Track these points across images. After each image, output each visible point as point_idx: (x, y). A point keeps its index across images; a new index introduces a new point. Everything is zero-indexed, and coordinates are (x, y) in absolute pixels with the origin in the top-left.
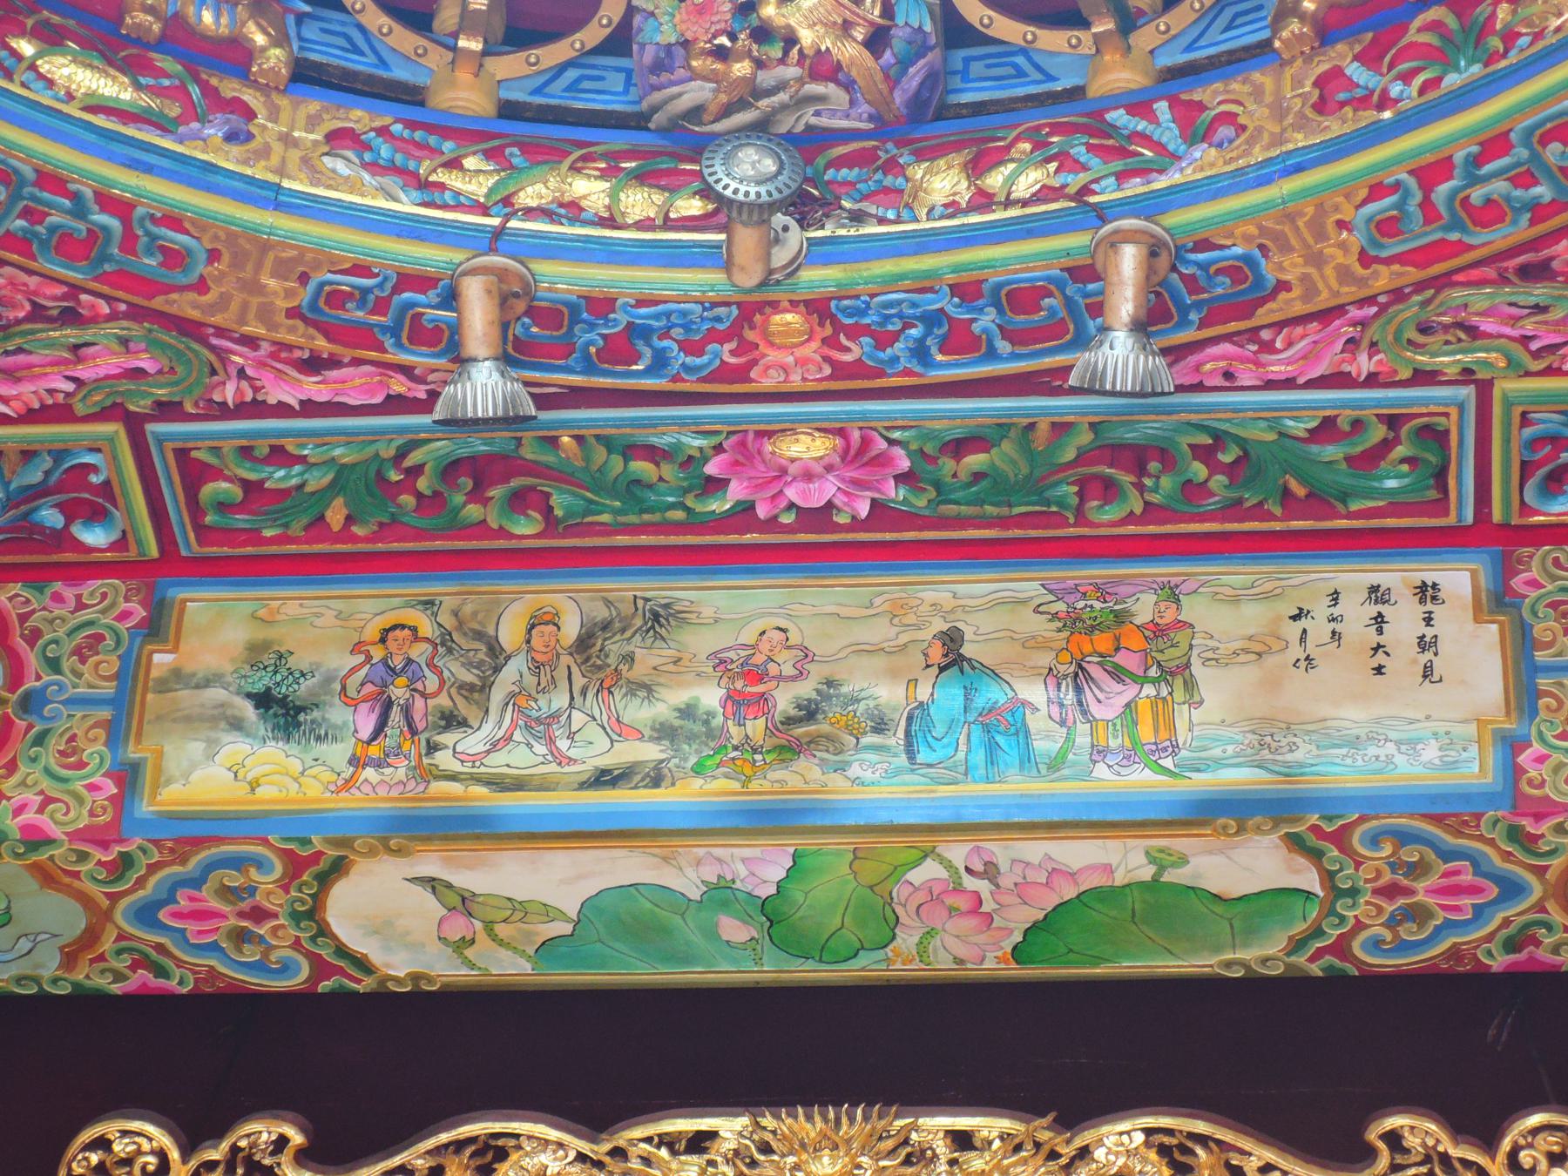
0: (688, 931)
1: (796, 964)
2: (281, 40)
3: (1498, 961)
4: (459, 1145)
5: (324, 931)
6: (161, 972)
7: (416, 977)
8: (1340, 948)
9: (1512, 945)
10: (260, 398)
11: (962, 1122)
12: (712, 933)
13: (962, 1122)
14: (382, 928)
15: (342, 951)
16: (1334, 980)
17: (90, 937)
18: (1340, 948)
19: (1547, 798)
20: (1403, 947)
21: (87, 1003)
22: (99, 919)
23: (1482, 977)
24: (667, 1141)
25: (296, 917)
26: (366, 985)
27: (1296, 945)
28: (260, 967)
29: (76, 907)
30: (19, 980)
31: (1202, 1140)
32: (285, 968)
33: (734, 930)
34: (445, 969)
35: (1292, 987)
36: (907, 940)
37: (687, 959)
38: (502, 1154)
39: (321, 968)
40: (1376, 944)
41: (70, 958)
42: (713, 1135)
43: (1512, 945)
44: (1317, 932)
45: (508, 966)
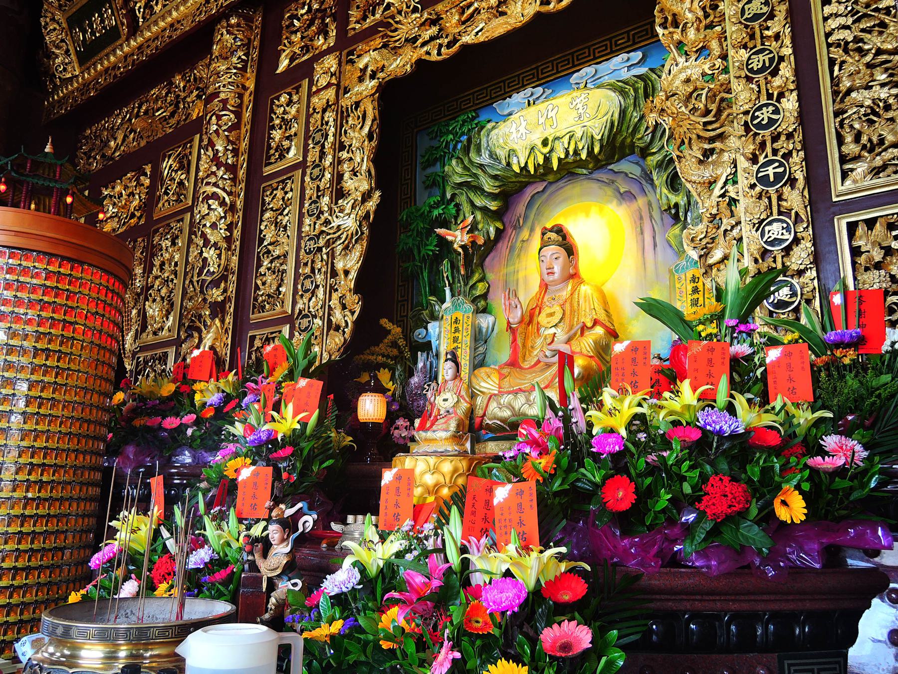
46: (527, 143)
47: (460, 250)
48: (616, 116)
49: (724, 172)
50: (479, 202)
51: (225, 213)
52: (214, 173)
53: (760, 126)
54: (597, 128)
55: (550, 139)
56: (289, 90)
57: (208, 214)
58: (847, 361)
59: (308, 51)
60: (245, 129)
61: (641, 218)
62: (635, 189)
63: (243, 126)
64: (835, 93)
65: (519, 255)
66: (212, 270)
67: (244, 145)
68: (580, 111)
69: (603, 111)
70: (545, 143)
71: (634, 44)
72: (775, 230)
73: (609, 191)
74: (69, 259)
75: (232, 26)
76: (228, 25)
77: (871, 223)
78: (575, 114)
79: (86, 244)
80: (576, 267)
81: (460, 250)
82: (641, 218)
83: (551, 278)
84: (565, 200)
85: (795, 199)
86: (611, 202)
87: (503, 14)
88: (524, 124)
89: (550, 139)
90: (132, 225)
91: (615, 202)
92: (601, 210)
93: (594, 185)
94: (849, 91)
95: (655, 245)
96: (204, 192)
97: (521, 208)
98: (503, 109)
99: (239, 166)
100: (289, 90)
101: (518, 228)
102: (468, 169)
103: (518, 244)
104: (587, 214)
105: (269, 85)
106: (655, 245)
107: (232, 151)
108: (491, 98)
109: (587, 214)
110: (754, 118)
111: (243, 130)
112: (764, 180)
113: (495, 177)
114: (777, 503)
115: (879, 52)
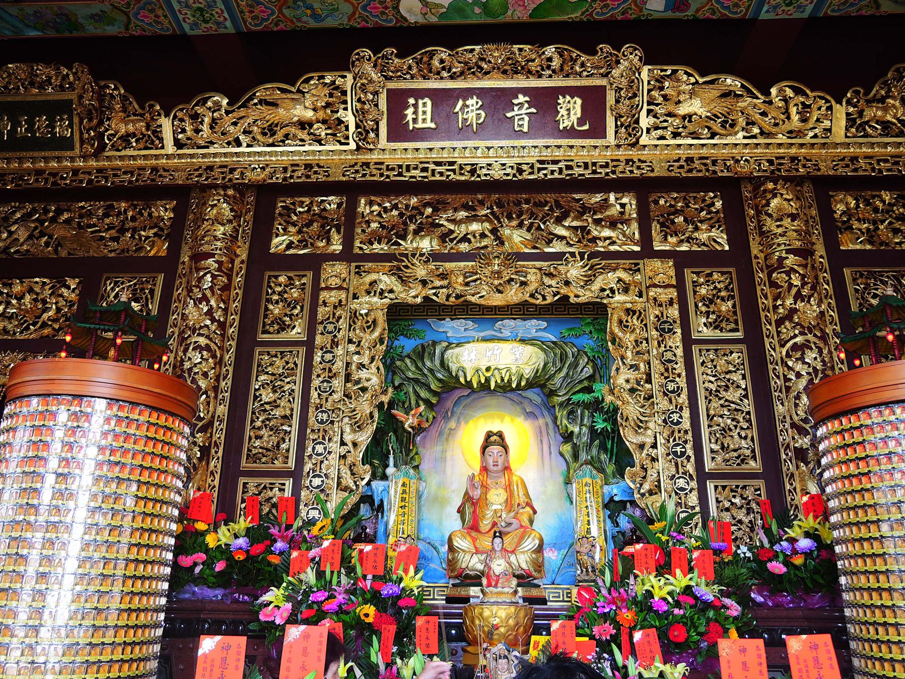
0: (468, 10)
1: (488, 19)
2: (892, 332)
3: (620, 18)
4: (426, 52)
5: (399, 12)
6: (367, 22)
7: (416, 22)
8: (591, 15)
9: (623, 14)
10: (244, 533)
11: (521, 46)
12: (473, 11)
13: (521, 46)
14: (410, 11)
15: (402, 16)
16: (589, 22)
17: (354, 14)
18: (591, 15)
19: (812, 91)
20: (603, 14)
21: (352, 29)
22: (356, 8)
23: (617, 21)
24: (466, 50)
25: (394, 8)
26: (406, 25)
27: (583, 13)
28: (386, 21)
29: (351, 6)
30: (340, 24)
31: (566, 49)
32: (391, 21)
33: (477, 10)
34: (421, 20)
35: (581, 22)
36: (510, 13)
37: (467, 17)
38: (434, 55)
39: (398, 21)
40: (598, 13)
41: (349, 20)
42: (474, 50)
43: (623, 14)
44: (587, 10)
45: (433, 19)
46: (475, 365)
47: (410, 430)
48: (542, 364)
49: (649, 441)
50: (424, 394)
51: (215, 365)
52: (207, 326)
53: (672, 422)
54: (528, 372)
55: (493, 368)
56: (291, 274)
57: (200, 363)
58: (726, 560)
59: (305, 247)
60: (237, 292)
61: (541, 432)
62: (537, 413)
63: (232, 289)
64: (708, 415)
65: (447, 440)
66: (202, 415)
67: (235, 305)
68: (517, 356)
69: (534, 360)
70: (488, 369)
71: (540, 314)
72: (681, 483)
73: (518, 409)
74: (165, 412)
75: (228, 196)
76: (225, 195)
77: (724, 487)
78: (513, 357)
79: (179, 398)
80: (508, 462)
81: (410, 430)
82: (541, 432)
83: (495, 468)
84: (484, 407)
85: (690, 468)
86: (520, 416)
87: (500, 292)
88: (474, 352)
89: (493, 368)
90: (44, 335)
91: (522, 417)
92: (512, 420)
93: (508, 402)
94: (714, 416)
95: (550, 453)
96: (196, 342)
97: (449, 404)
98: (439, 327)
99: (228, 324)
100: (291, 274)
101: (446, 418)
102: (421, 370)
103: (447, 431)
104: (502, 421)
105: (262, 262)
106: (550, 453)
107: (223, 310)
108: (427, 315)
109: (502, 421)
110: (670, 418)
111: (233, 293)
112: (675, 453)
113: (440, 380)
114: (367, 620)
115: (726, 400)
